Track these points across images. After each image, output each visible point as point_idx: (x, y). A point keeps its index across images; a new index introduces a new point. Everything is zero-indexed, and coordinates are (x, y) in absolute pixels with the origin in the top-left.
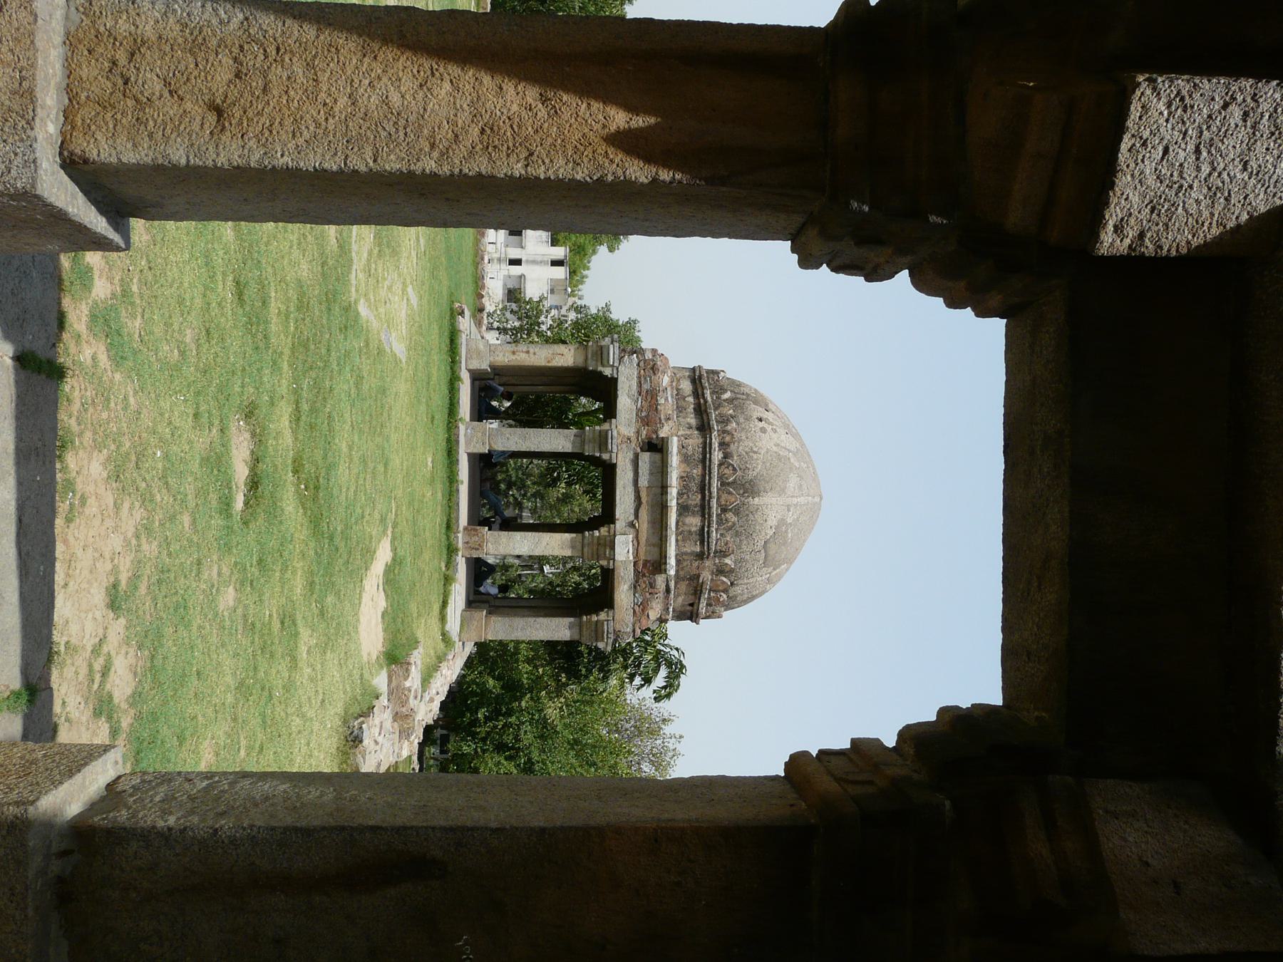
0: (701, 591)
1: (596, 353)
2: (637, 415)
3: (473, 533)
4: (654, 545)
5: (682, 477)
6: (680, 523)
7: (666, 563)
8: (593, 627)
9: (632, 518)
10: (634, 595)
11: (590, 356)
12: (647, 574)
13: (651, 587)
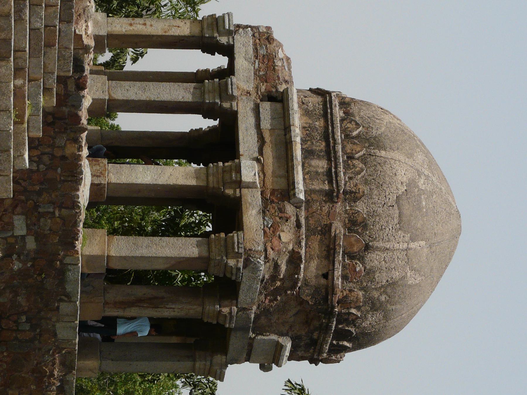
0: (335, 249)
1: (212, 24)
2: (255, 74)
3: (94, 163)
4: (280, 177)
5: (304, 128)
6: (306, 165)
7: (294, 188)
8: (222, 242)
9: (256, 155)
10: (264, 218)
11: (205, 26)
12: (275, 200)
13: (281, 212)
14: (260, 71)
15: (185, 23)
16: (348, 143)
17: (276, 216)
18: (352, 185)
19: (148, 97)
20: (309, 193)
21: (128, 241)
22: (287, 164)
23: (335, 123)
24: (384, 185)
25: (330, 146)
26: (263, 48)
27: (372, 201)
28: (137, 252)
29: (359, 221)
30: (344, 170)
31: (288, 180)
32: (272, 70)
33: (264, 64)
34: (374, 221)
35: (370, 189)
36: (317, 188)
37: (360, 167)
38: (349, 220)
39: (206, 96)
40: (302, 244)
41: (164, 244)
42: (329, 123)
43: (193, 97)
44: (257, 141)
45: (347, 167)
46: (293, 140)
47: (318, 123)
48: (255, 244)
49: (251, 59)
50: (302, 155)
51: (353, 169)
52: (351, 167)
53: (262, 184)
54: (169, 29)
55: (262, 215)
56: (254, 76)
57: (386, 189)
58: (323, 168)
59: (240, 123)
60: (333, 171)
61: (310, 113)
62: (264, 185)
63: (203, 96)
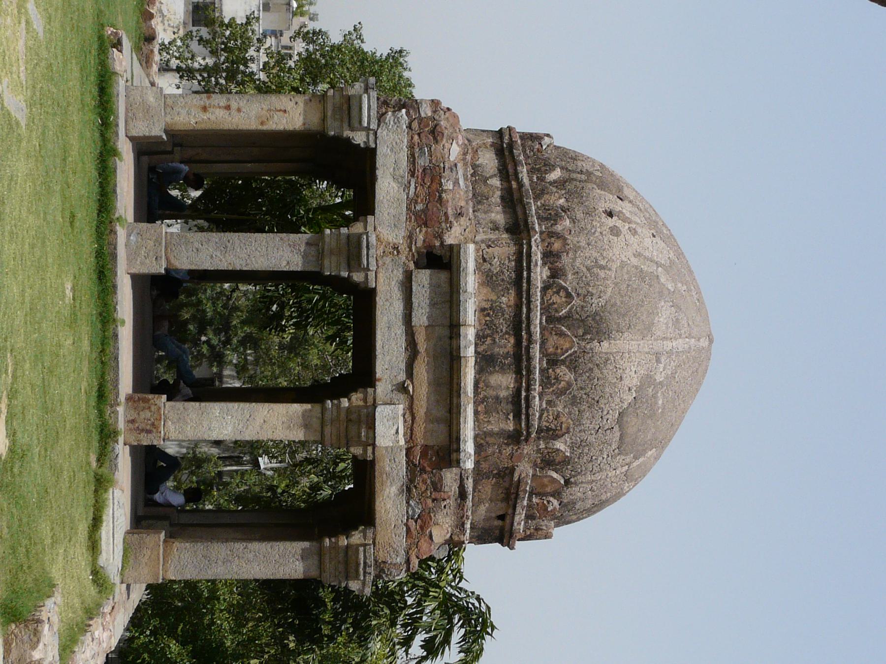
5: (483, 310)
6: (481, 385)
7: (458, 450)
8: (342, 555)
9: (402, 377)
10: (408, 502)
11: (329, 114)
12: (428, 469)
14: (416, 202)
15: (296, 103)
16: (551, 333)
17: (428, 497)
18: (551, 417)
19: (230, 264)
20: (483, 437)
21: (195, 552)
22: (450, 396)
23: (533, 300)
24: (602, 401)
25: (522, 347)
26: (425, 154)
27: (580, 429)
28: (209, 572)
29: (557, 461)
30: (541, 387)
31: (450, 426)
32: (437, 202)
33: (423, 188)
34: (580, 453)
35: (579, 411)
36: (496, 429)
37: (567, 380)
38: (542, 460)
39: (325, 261)
40: (465, 526)
41: (251, 556)
42: (524, 300)
43: (304, 262)
44: (405, 348)
45: (546, 382)
46: (462, 355)
47: (506, 299)
48: (392, 553)
49: (403, 177)
50: (477, 366)
51: (554, 385)
52: (553, 381)
53: (409, 434)
54: (268, 115)
55: (407, 496)
56: (407, 214)
57: (604, 407)
58: (508, 388)
59: (378, 313)
60: (523, 397)
61: (494, 278)
62: (411, 437)
63: (321, 259)
